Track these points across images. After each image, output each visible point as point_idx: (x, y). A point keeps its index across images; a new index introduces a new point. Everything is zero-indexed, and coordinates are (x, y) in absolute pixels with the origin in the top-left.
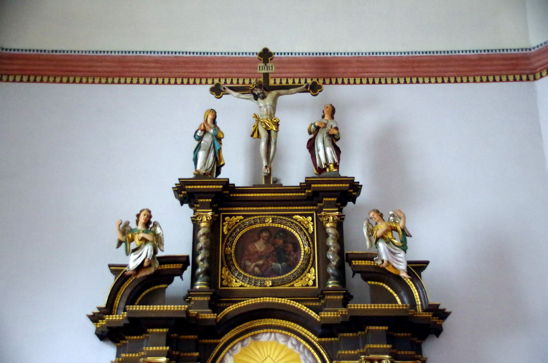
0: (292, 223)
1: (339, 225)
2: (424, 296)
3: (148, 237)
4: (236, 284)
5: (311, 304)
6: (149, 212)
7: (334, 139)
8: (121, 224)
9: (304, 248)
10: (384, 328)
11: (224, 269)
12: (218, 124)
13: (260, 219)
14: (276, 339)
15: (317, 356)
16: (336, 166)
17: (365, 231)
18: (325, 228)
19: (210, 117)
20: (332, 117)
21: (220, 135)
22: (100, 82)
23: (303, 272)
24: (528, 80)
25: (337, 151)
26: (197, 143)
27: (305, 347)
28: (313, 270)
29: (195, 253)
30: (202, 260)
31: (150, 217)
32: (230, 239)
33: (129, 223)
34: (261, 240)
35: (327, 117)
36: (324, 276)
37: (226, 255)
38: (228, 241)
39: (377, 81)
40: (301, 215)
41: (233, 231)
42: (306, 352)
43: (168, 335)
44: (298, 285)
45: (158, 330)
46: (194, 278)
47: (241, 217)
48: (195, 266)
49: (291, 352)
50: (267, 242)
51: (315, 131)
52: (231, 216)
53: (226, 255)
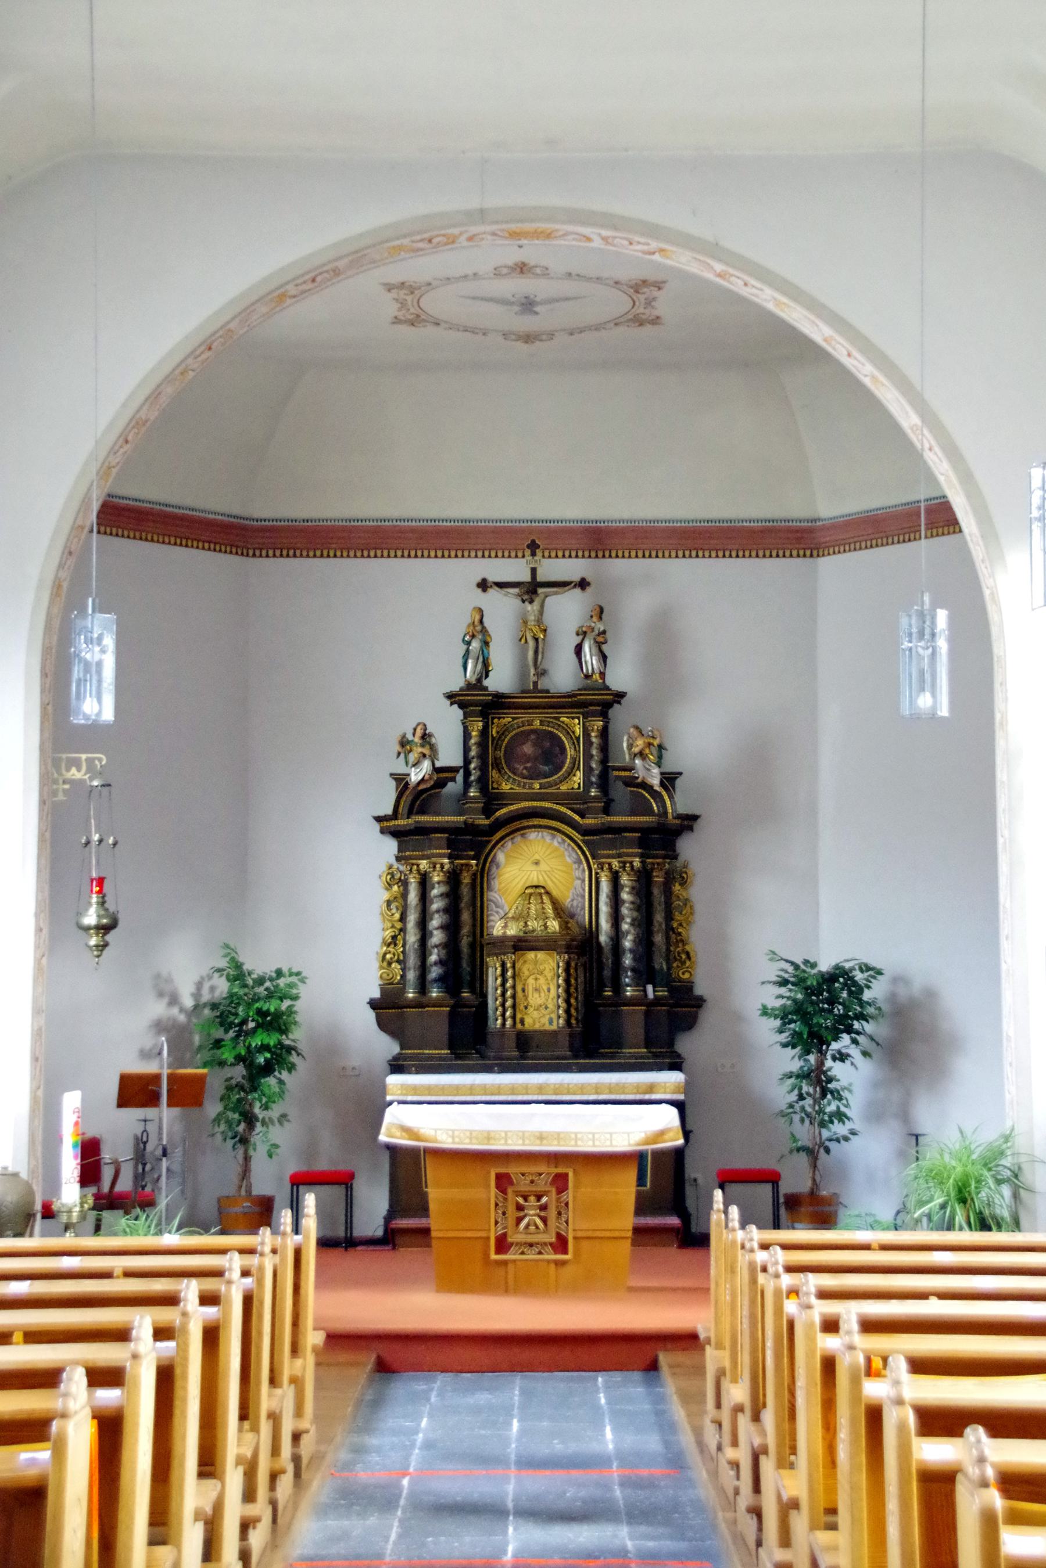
0: (559, 725)
1: (604, 733)
2: (503, 1060)
3: (426, 751)
4: (506, 787)
5: (575, 806)
6: (425, 725)
7: (599, 645)
9: (570, 752)
10: (637, 834)
11: (494, 771)
12: (486, 625)
13: (528, 721)
14: (543, 837)
15: (580, 853)
16: (602, 675)
17: (625, 745)
18: (589, 735)
19: (477, 618)
20: (600, 618)
21: (488, 639)
22: (355, 556)
23: (566, 778)
24: (811, 556)
25: (604, 658)
26: (465, 647)
27: (569, 845)
28: (578, 772)
29: (467, 761)
30: (474, 769)
31: (426, 729)
32: (500, 742)
33: (405, 734)
34: (530, 743)
35: (595, 619)
36: (587, 784)
37: (496, 759)
38: (497, 744)
39: (654, 554)
40: (568, 717)
41: (502, 734)
42: (570, 849)
43: (448, 839)
44: (564, 788)
45: (439, 835)
46: (467, 785)
47: (510, 719)
48: (467, 774)
49: (556, 849)
50: (535, 745)
51: (583, 634)
52: (499, 718)
53: (496, 759)
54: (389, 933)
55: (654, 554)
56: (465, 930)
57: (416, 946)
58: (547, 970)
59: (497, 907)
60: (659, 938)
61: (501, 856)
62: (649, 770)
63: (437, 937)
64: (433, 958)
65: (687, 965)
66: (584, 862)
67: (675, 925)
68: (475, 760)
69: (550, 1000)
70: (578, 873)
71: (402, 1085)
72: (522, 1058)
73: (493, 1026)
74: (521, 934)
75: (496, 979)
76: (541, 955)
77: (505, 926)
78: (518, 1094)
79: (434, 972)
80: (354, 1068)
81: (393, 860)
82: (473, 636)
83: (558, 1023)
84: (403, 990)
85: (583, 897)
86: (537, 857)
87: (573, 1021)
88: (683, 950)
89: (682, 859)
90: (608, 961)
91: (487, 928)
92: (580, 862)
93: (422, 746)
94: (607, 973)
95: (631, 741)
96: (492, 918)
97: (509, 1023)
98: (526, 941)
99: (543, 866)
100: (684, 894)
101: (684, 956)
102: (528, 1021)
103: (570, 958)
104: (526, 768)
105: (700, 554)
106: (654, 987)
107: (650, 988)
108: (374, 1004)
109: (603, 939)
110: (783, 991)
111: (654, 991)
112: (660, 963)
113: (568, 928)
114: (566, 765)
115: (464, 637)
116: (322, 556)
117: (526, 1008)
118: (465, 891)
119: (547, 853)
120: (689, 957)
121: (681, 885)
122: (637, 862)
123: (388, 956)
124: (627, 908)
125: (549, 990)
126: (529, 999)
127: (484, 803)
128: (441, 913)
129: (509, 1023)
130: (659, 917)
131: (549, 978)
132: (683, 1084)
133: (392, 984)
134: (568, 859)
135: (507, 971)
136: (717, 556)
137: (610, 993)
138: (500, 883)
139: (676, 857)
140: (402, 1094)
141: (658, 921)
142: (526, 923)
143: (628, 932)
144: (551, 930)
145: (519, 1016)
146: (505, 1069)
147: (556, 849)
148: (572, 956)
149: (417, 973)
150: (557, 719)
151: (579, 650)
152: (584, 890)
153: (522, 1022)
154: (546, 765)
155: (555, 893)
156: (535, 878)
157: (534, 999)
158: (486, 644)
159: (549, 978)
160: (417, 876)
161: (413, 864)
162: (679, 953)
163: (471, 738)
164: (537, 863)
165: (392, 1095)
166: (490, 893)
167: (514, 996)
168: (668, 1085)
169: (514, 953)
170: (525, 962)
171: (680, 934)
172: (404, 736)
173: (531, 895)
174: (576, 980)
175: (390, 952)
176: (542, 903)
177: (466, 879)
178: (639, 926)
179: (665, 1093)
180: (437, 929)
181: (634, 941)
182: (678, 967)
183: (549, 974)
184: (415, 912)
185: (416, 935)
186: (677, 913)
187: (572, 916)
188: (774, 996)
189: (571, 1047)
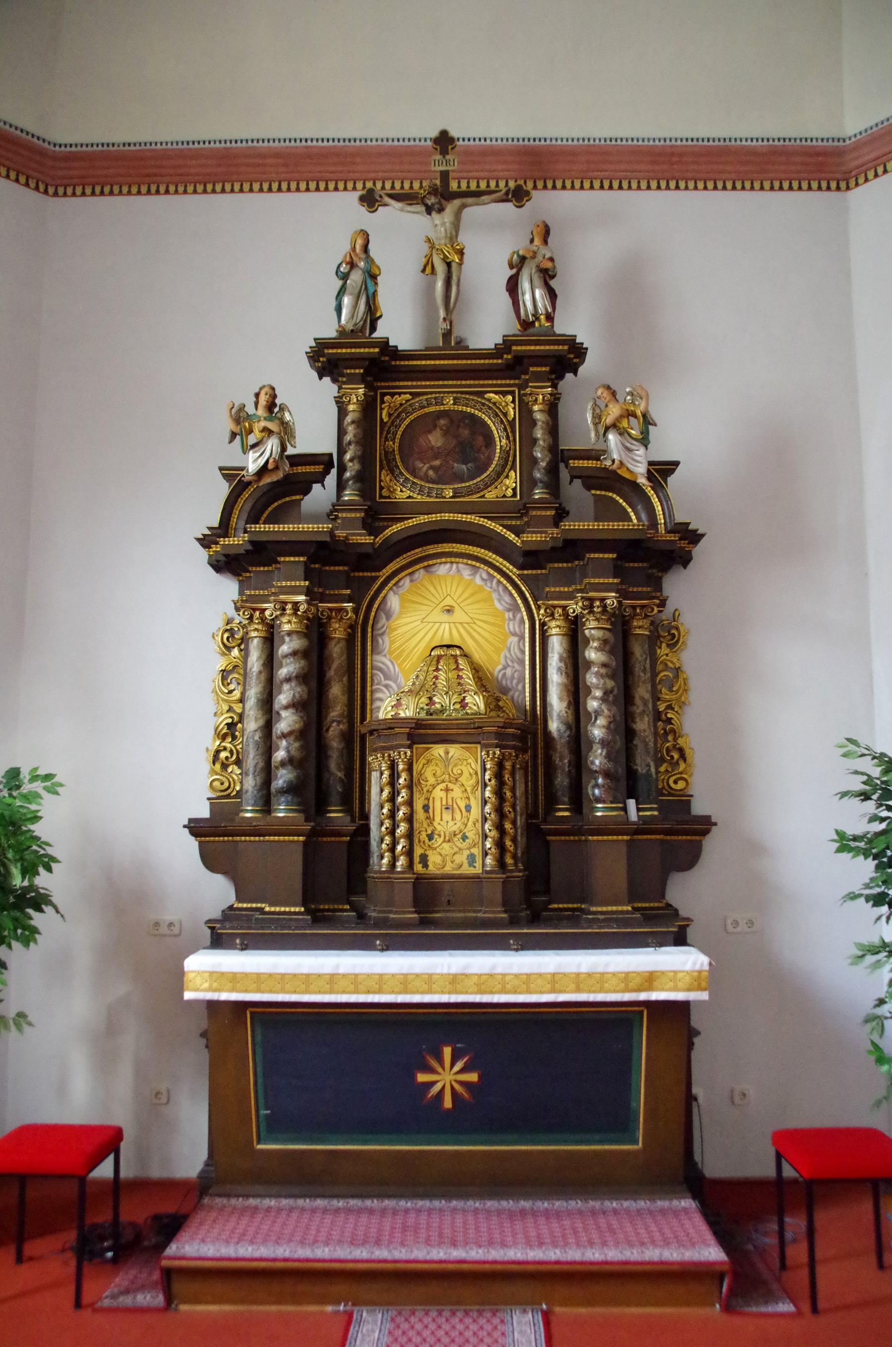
0: (483, 404)
4: (402, 494)
6: (273, 389)
8: (232, 408)
9: (500, 442)
12: (372, 254)
13: (435, 398)
14: (458, 570)
16: (550, 318)
19: (360, 242)
20: (545, 242)
22: (195, 192)
24: (838, 188)
25: (552, 295)
26: (340, 283)
27: (499, 582)
30: (351, 460)
32: (393, 429)
35: (537, 242)
36: (528, 483)
39: (616, 184)
40: (496, 393)
42: (501, 589)
44: (491, 495)
47: (408, 396)
48: (342, 469)
49: (480, 589)
50: (446, 433)
51: (518, 263)
52: (393, 395)
54: (225, 719)
55: (616, 184)
56: (336, 711)
57: (257, 738)
58: (466, 774)
59: (387, 677)
60: (642, 725)
61: (394, 601)
62: (629, 450)
63: (287, 721)
64: (280, 755)
65: (681, 769)
66: (523, 609)
67: (662, 708)
68: (352, 447)
69: (470, 824)
70: (513, 626)
71: (211, 973)
72: (424, 923)
73: (376, 868)
74: (423, 715)
75: (382, 791)
76: (455, 750)
77: (398, 705)
78: (412, 993)
79: (283, 777)
80: (171, 924)
81: (232, 612)
82: (352, 265)
83: (484, 865)
84: (238, 808)
85: (522, 662)
86: (449, 601)
87: (509, 860)
88: (674, 746)
89: (670, 607)
90: (563, 760)
91: (371, 710)
92: (515, 608)
93: (269, 419)
94: (562, 780)
95: (598, 411)
96: (378, 695)
97: (401, 862)
98: (430, 727)
99: (459, 615)
100: (675, 660)
101: (676, 756)
102: (434, 859)
103: (503, 754)
104: (432, 468)
105: (682, 184)
106: (637, 803)
107: (631, 803)
108: (196, 828)
109: (554, 726)
110: (870, 806)
111: (639, 810)
112: (643, 764)
113: (499, 708)
114: (495, 462)
115: (339, 267)
116: (149, 192)
117: (430, 837)
118: (336, 650)
119: (466, 595)
120: (683, 756)
121: (671, 646)
122: (612, 599)
123: (223, 755)
124: (597, 673)
125: (468, 808)
126: (435, 824)
127: (365, 511)
128: (293, 684)
129: (401, 862)
130: (642, 692)
131: (469, 789)
132: (705, 974)
133: (228, 796)
134: (498, 605)
135: (399, 777)
136: (705, 188)
137: (567, 814)
138: (392, 642)
139: (663, 604)
140: (211, 989)
141: (642, 698)
142: (430, 698)
143: (597, 713)
144: (472, 709)
145: (418, 851)
146: (392, 944)
147: (480, 589)
148: (507, 751)
149: (259, 780)
150: (481, 394)
151: (513, 286)
152: (523, 652)
153: (424, 859)
154: (466, 464)
155: (478, 656)
156: (446, 633)
157: (445, 823)
158: (372, 276)
159: (469, 789)
160: (260, 627)
161: (254, 610)
162: (668, 750)
163: (346, 433)
164: (449, 611)
165: (197, 990)
166: (377, 657)
167: (410, 819)
168: (680, 975)
169: (410, 747)
170: (429, 761)
171: (669, 721)
172: (242, 408)
173: (439, 657)
174: (513, 790)
175: (225, 749)
176: (457, 668)
177: (338, 631)
178: (614, 703)
179: (675, 989)
180: (286, 708)
181: (608, 728)
182: (667, 771)
183: (469, 782)
184: (257, 685)
185: (256, 720)
186: (664, 690)
187: (505, 691)
188: (866, 819)
189: (506, 904)
